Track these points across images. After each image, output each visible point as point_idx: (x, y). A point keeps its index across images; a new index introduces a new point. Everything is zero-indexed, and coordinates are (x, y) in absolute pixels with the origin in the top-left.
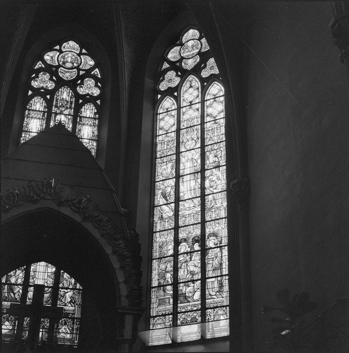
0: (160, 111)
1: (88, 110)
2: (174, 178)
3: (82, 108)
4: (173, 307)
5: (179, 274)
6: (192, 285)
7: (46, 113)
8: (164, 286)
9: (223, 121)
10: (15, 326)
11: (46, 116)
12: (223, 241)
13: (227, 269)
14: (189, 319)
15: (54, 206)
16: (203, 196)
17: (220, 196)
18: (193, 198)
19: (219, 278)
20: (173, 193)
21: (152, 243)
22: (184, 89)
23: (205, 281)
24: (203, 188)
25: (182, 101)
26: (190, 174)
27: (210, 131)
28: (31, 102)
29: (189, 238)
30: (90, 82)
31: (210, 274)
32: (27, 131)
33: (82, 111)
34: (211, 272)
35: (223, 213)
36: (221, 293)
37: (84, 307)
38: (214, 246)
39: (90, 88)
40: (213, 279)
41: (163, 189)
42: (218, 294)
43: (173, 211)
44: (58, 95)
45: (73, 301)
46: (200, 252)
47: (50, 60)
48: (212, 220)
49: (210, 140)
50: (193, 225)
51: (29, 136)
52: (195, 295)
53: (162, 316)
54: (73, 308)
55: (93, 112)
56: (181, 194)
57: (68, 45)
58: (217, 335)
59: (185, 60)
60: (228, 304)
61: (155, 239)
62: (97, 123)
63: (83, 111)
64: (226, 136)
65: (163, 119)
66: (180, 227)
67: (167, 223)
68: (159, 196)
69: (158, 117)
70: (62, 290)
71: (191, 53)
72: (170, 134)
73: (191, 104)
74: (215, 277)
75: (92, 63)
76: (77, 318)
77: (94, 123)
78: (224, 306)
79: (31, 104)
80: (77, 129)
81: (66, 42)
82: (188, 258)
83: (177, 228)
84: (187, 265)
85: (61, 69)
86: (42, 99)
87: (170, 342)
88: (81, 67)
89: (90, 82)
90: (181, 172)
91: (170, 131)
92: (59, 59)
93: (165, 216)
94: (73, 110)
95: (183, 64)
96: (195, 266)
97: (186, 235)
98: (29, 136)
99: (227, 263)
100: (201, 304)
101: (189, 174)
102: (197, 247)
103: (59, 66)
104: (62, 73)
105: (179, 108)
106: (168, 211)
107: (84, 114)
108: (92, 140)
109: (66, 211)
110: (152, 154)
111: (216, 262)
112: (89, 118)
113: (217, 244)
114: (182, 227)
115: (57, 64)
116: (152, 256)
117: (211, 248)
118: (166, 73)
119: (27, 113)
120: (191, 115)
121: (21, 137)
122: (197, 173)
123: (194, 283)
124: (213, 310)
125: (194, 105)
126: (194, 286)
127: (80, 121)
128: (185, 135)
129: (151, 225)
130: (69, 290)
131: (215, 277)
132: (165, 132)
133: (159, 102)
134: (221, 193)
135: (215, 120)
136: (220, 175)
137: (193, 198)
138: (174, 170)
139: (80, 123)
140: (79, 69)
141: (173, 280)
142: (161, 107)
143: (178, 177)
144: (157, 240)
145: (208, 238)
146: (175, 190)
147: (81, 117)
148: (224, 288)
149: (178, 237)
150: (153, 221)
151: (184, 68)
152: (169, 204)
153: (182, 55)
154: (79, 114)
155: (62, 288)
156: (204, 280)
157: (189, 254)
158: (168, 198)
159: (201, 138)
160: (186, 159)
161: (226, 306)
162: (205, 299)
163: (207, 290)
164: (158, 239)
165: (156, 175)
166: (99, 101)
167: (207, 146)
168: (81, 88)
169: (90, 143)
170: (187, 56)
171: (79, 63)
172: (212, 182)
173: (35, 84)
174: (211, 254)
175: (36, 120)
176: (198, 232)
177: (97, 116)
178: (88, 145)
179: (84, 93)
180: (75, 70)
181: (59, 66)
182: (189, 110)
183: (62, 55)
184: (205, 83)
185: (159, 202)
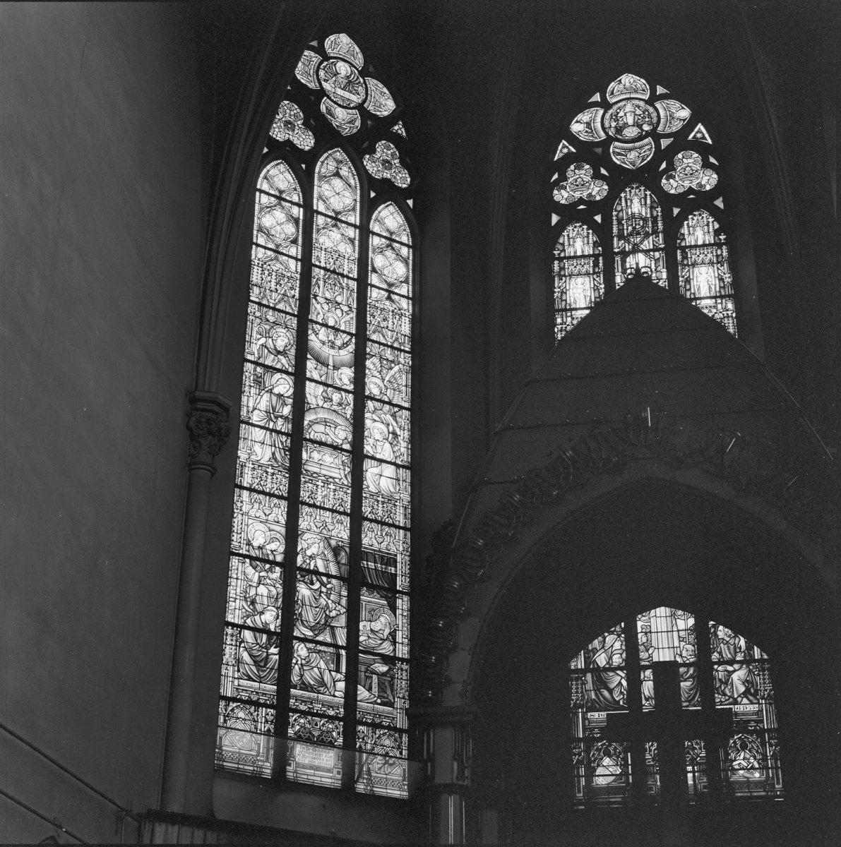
1: (698, 229)
3: (682, 226)
11: (601, 265)
28: (561, 240)
32: (566, 310)
33: (683, 235)
44: (619, 208)
47: (586, 132)
54: (755, 708)
55: (711, 230)
57: (621, 86)
62: (725, 254)
63: (686, 232)
75: (685, 113)
76: (769, 731)
77: (717, 256)
79: (563, 244)
80: (681, 279)
85: (615, 147)
86: (585, 227)
89: (689, 161)
92: (607, 125)
103: (609, 140)
107: (690, 240)
108: (722, 297)
115: (603, 136)
119: (556, 268)
121: (555, 325)
130: (737, 666)
147: (683, 249)
155: (720, 663)
169: (719, 306)
171: (655, 120)
178: (714, 311)
179: (681, 190)
180: (649, 140)
181: (609, 140)
183: (611, 111)
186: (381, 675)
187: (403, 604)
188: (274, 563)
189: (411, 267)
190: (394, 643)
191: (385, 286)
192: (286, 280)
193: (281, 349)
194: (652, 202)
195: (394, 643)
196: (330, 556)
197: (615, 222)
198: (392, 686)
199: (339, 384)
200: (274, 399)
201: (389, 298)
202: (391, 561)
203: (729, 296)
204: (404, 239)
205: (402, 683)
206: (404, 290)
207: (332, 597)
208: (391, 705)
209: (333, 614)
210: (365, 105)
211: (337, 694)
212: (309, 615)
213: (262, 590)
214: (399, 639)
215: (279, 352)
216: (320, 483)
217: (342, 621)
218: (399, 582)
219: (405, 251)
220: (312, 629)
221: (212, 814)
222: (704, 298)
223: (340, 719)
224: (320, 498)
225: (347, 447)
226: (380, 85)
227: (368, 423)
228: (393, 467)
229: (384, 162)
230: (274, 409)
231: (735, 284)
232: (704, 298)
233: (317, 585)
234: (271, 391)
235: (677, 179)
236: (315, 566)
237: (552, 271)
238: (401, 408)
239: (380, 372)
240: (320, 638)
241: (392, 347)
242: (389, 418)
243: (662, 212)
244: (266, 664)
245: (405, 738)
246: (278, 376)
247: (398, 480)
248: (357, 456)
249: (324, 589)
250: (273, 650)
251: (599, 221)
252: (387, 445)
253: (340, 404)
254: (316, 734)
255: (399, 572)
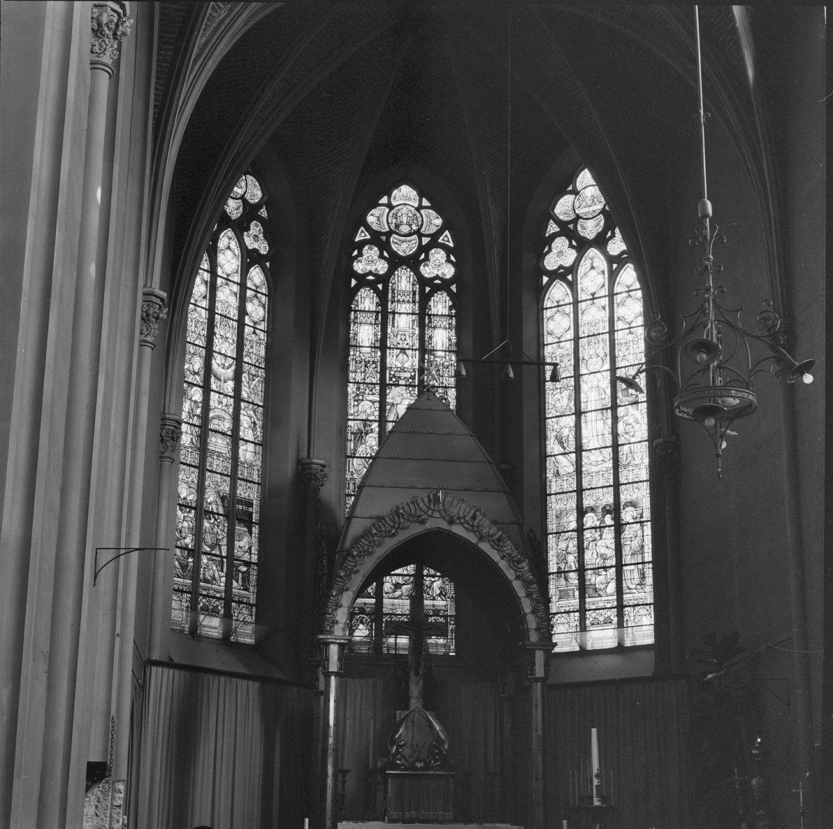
0: (547, 304)
1: (439, 304)
2: (573, 414)
3: (430, 300)
4: (580, 602)
5: (586, 557)
6: (604, 573)
7: (380, 314)
8: (564, 572)
9: (641, 331)
10: (371, 629)
11: (380, 319)
12: (644, 515)
13: (651, 554)
14: (601, 619)
15: (443, 525)
16: (615, 446)
17: (639, 447)
18: (602, 448)
19: (640, 566)
20: (572, 438)
21: (546, 511)
22: (582, 270)
23: (622, 569)
24: (615, 435)
25: (579, 291)
26: (596, 410)
27: (624, 345)
28: (356, 298)
29: (598, 507)
30: (438, 255)
31: (627, 559)
32: (356, 346)
33: (430, 306)
34: (629, 557)
35: (644, 474)
36: (643, 586)
37: (458, 601)
38: (632, 521)
39: (439, 266)
40: (633, 567)
41: (558, 430)
42: (639, 587)
43: (573, 465)
44: (393, 282)
45: (444, 593)
46: (613, 528)
47: (377, 223)
48: (629, 483)
49: (623, 360)
50: (602, 487)
51: (360, 353)
52: (608, 587)
53: (565, 612)
54: (444, 603)
55: (447, 306)
56: (584, 441)
57: (401, 194)
58: (639, 642)
59: (581, 220)
60: (652, 601)
61: (550, 505)
62: (454, 323)
63: (432, 305)
64: (646, 356)
65: (551, 318)
66: (585, 490)
67: (565, 482)
68: (552, 441)
69: (545, 314)
70: (428, 579)
71: (591, 209)
72: (563, 343)
73: (594, 297)
74: (635, 564)
75: (439, 222)
76: (450, 616)
77: (449, 324)
78: (647, 604)
79: (357, 301)
80: (426, 336)
81: (397, 187)
82: (597, 535)
83: (580, 491)
84: (596, 545)
85: (394, 238)
86: (372, 291)
87: (577, 649)
88: (423, 229)
89: (438, 255)
90: (583, 406)
91: (564, 339)
92: (390, 221)
93: (562, 471)
94: (417, 304)
95: (579, 228)
96: (608, 547)
97: (594, 503)
98: (360, 353)
99: (650, 546)
100: (618, 600)
101: (594, 411)
102: (609, 520)
103: (390, 233)
104: (396, 243)
105: (576, 303)
106: (566, 465)
107: (434, 311)
108: (450, 351)
109: (458, 530)
110: (539, 376)
111: (636, 544)
112: (442, 315)
113: (636, 518)
114: (587, 489)
115: (388, 229)
116: (546, 529)
117: (628, 523)
118: (553, 240)
119: (352, 317)
120: (594, 316)
121: (349, 355)
122: (607, 409)
123: (606, 571)
124: (632, 608)
125: (597, 300)
126: (606, 575)
127: (430, 322)
128: (586, 347)
129: (543, 483)
130: (436, 578)
131: (635, 564)
132: (556, 340)
133: (545, 290)
134: (640, 444)
135: (630, 328)
136: (639, 417)
137: (602, 448)
138: (573, 403)
139: (430, 325)
140: (420, 235)
141: (578, 565)
142: (549, 298)
143: (579, 413)
144: (553, 507)
145: (624, 509)
146: (576, 434)
147: (430, 316)
148: (647, 579)
149: (582, 504)
150: (546, 478)
151: (581, 234)
152: (567, 454)
153: (577, 212)
154: (427, 310)
155: (427, 576)
156: (619, 567)
157: (598, 530)
158: (565, 445)
159: (611, 354)
160: (589, 385)
161: (650, 604)
162: (622, 594)
163: (624, 581)
164: (554, 505)
165: (547, 408)
166: (455, 286)
167: (619, 368)
168: (426, 267)
169: (447, 357)
170: (585, 214)
171: (420, 223)
172: (628, 426)
173: (359, 267)
174: (628, 532)
175: (366, 327)
176: (609, 499)
177: (453, 311)
178: (444, 360)
179: (432, 276)
180: (415, 237)
181: (390, 233)
182: (590, 306)
183: (393, 211)
184: (615, 263)
185: (552, 450)
186: (243, 573)
187: (255, 530)
188: (191, 508)
189: (266, 309)
190: (250, 554)
191: (252, 324)
192: (200, 324)
193: (196, 371)
194: (414, 280)
195: (250, 554)
196: (220, 503)
197: (390, 291)
198: (249, 579)
199: (226, 392)
200: (193, 403)
201: (254, 333)
202: (250, 504)
203: (454, 351)
204: (264, 291)
205: (253, 578)
206: (263, 326)
207: (220, 527)
208: (247, 590)
209: (220, 537)
210: (245, 196)
211: (221, 584)
212: (209, 538)
213: (185, 524)
214: (253, 552)
215: (195, 373)
216: (215, 457)
217: (225, 542)
218: (254, 517)
219: (264, 299)
220: (209, 547)
221: (171, 660)
222: (439, 351)
223: (222, 599)
224: (215, 467)
225: (229, 433)
226: (254, 180)
227: (242, 417)
228: (253, 445)
229: (256, 240)
230: (192, 410)
231: (457, 344)
232: (439, 351)
233: (212, 521)
234: (191, 399)
235: (430, 267)
236: (212, 509)
237: (349, 318)
238: (258, 406)
239: (248, 383)
240: (213, 552)
241: (255, 366)
242: (252, 413)
243: (419, 288)
244: (187, 568)
245: (254, 609)
246: (195, 388)
247: (255, 453)
248: (235, 438)
249: (216, 523)
250: (190, 560)
251: (381, 289)
252: (250, 430)
253: (227, 406)
254: (211, 608)
255: (254, 511)
